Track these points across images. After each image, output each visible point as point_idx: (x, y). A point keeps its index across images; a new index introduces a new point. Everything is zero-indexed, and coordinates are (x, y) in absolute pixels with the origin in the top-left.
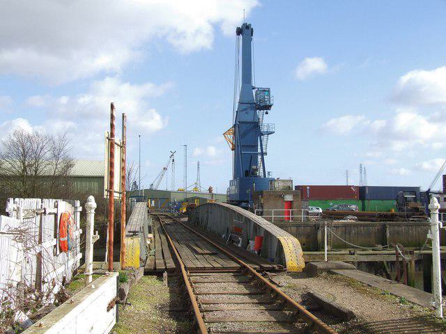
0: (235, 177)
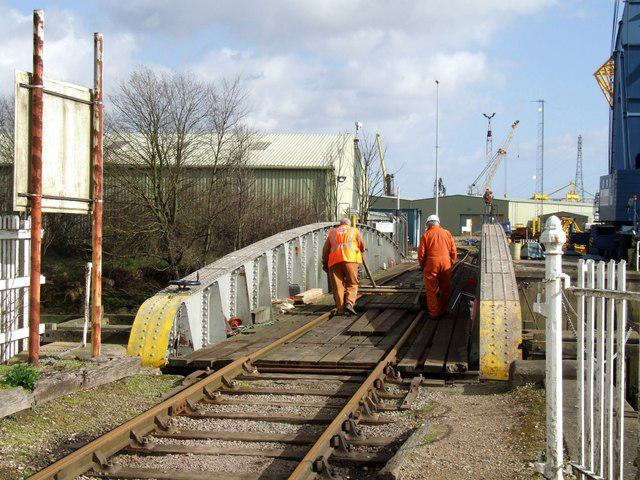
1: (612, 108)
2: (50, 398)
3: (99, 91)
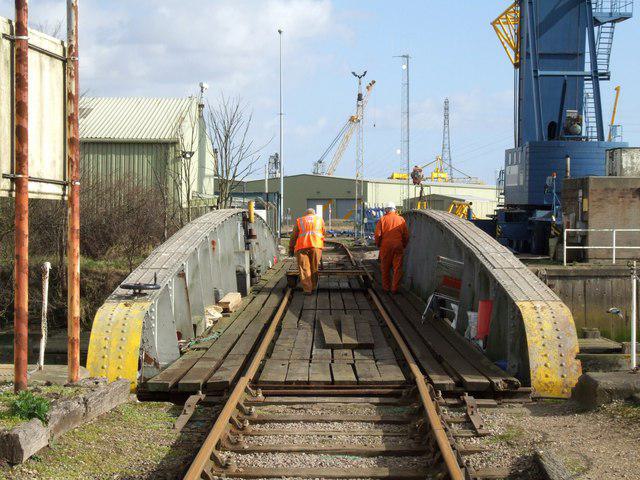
0: (520, 142)
1: (516, 66)
2: (61, 433)
3: (74, 43)
